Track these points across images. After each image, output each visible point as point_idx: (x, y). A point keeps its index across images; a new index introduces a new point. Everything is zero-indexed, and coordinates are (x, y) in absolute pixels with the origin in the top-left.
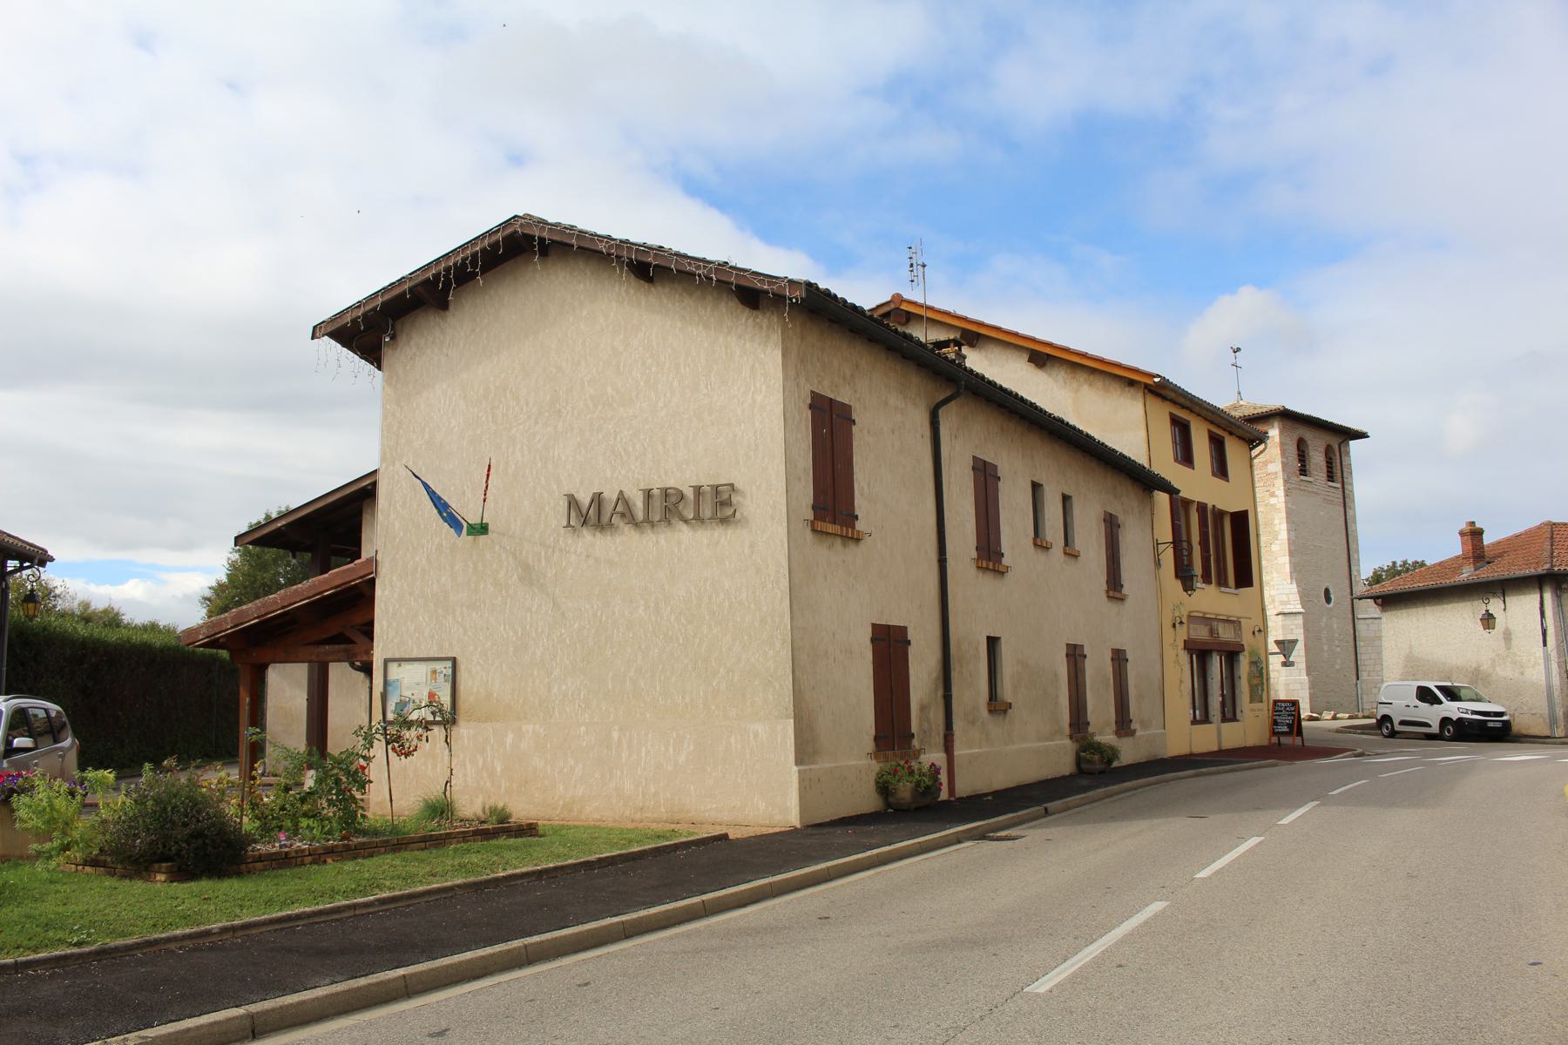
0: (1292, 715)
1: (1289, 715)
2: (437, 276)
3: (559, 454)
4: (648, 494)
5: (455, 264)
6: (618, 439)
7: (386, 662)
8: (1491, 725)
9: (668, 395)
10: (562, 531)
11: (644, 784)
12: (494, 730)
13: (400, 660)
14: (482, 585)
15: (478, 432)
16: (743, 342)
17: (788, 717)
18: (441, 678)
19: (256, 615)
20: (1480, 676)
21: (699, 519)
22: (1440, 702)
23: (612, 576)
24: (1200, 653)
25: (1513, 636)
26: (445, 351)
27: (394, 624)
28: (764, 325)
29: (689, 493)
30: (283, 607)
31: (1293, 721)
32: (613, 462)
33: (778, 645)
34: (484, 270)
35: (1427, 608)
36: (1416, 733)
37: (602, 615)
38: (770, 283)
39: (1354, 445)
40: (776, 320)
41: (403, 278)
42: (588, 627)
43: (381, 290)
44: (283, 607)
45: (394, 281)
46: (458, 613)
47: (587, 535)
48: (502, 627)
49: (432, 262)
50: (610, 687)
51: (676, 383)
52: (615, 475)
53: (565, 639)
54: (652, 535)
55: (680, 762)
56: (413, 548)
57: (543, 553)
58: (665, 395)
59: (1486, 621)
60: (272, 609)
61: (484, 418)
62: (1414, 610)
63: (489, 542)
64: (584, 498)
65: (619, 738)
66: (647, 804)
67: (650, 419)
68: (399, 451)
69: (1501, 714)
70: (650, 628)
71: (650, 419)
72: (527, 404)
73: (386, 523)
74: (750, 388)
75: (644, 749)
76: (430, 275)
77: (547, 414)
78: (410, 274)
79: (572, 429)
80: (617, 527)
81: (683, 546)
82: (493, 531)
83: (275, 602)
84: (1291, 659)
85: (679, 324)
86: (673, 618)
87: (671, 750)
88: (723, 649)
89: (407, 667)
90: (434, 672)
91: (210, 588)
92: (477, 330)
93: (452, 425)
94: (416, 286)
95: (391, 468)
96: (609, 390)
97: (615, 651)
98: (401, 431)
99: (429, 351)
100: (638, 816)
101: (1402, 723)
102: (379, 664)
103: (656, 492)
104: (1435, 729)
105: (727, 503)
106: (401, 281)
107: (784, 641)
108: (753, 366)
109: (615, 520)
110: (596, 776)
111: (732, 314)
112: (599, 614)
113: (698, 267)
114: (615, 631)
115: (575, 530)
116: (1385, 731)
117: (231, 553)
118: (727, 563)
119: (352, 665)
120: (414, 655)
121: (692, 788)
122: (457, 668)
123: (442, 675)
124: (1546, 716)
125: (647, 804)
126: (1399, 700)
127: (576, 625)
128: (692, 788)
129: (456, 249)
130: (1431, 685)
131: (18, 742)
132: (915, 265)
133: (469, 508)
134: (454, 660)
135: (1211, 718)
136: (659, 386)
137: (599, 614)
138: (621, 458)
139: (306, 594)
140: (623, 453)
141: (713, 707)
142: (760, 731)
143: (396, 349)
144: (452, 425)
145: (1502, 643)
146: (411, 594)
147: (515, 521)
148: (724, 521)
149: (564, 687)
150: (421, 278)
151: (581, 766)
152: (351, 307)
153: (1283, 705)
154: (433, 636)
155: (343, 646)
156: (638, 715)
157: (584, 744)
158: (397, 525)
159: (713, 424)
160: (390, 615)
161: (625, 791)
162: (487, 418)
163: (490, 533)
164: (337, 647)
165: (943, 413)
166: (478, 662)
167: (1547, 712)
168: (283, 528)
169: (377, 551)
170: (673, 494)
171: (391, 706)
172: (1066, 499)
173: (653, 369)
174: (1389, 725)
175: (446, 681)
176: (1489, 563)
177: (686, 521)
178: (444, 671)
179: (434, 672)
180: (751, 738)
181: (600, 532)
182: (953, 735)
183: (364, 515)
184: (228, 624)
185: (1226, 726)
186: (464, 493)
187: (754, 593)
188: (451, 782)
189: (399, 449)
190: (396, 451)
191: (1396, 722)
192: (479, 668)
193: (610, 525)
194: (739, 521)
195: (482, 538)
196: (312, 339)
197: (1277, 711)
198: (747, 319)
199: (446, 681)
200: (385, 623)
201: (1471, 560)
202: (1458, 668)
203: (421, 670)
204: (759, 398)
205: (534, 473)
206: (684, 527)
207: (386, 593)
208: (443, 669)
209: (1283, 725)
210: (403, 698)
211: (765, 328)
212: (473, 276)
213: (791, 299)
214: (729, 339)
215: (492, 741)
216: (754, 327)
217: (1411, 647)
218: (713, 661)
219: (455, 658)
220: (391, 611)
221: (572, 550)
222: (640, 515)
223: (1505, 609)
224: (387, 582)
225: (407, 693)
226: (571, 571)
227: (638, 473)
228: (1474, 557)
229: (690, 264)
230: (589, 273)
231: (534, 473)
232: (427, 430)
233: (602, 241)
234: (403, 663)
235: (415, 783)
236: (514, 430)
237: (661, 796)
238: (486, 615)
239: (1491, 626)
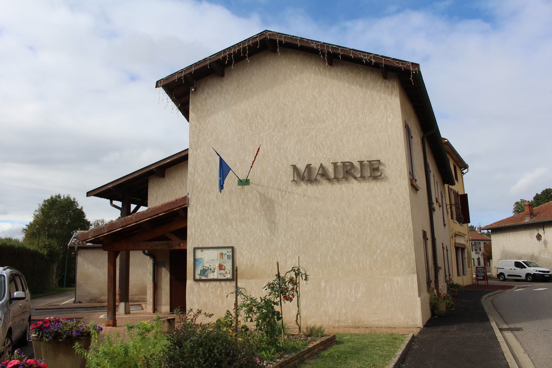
0: (484, 273)
1: (483, 273)
2: (224, 58)
3: (286, 146)
4: (335, 164)
5: (234, 52)
6: (318, 139)
7: (195, 249)
8: (546, 276)
9: (343, 118)
10: (290, 183)
11: (339, 308)
12: (256, 283)
13: (202, 249)
14: (247, 210)
15: (243, 135)
16: (380, 94)
17: (414, 273)
18: (225, 257)
19: (121, 226)
20: (534, 258)
21: (363, 177)
22: (525, 268)
23: (318, 205)
24: (457, 249)
25: (548, 243)
26: (223, 95)
27: (199, 230)
28: (390, 86)
29: (357, 165)
30: (136, 222)
31: (485, 275)
32: (315, 150)
33: (407, 238)
34: (250, 55)
35: (511, 233)
36: (517, 279)
37: (313, 225)
38: (402, 64)
40: (395, 84)
41: (206, 58)
43: (193, 64)
44: (136, 222)
45: (201, 60)
46: (234, 224)
48: (259, 231)
49: (221, 51)
50: (319, 260)
51: (346, 112)
52: (317, 156)
53: (294, 236)
54: (338, 185)
55: (358, 297)
56: (208, 192)
57: (280, 195)
58: (341, 118)
60: (130, 223)
61: (245, 128)
62: (505, 234)
63: (250, 189)
64: (302, 167)
65: (325, 286)
66: (341, 319)
67: (334, 129)
68: (199, 144)
69: (548, 272)
70: (339, 231)
71: (334, 129)
72: (269, 121)
73: (193, 179)
74: (385, 116)
75: (338, 291)
76: (221, 57)
77: (279, 126)
78: (210, 57)
79: (293, 134)
80: (319, 182)
81: (355, 191)
82: (253, 184)
83: (131, 219)
85: (347, 85)
86: (351, 226)
87: (353, 291)
88: (378, 240)
89: (206, 252)
90: (222, 254)
91: (26, 225)
92: (240, 86)
93: (228, 132)
94: (213, 62)
95: (195, 152)
96: (312, 115)
97: (321, 242)
98: (200, 135)
99: (214, 96)
100: (337, 325)
101: (509, 275)
102: (191, 250)
103: (339, 164)
104: (524, 277)
105: (377, 169)
106: (205, 60)
107: (410, 236)
108: (385, 105)
109: (319, 178)
110: (313, 305)
111: (373, 81)
113: (365, 56)
115: (297, 183)
116: (501, 279)
117: (35, 212)
118: (378, 198)
119: (144, 253)
120: (210, 245)
121: (365, 310)
122: (235, 252)
123: (226, 256)
125: (341, 319)
126: (508, 267)
127: (300, 230)
128: (365, 310)
129: (234, 45)
130: (521, 261)
131: (17, 294)
133: (239, 172)
134: (233, 248)
136: (338, 113)
138: (320, 148)
139: (149, 215)
140: (320, 145)
141: (374, 269)
142: (399, 280)
143: (196, 95)
144: (228, 132)
145: (543, 246)
146: (208, 215)
147: (264, 178)
148: (375, 178)
150: (215, 59)
151: (305, 300)
152: (177, 72)
153: (480, 269)
154: (220, 236)
155: (166, 242)
156: (335, 274)
157: (306, 289)
158: (199, 181)
159: (367, 132)
160: (196, 225)
161: (329, 312)
162: (247, 128)
163: (250, 184)
164: (162, 242)
166: (246, 249)
168: (111, 188)
169: (188, 193)
170: (348, 165)
171: (198, 272)
173: (335, 106)
174: (503, 277)
175: (228, 258)
176: (535, 216)
177: (355, 178)
178: (227, 254)
179: (222, 254)
180: (395, 284)
181: (310, 183)
182: (438, 281)
183: (149, 183)
184: (105, 230)
185: (464, 277)
186: (235, 165)
187: (393, 213)
188: (300, 314)
189: (199, 143)
190: (198, 144)
191: (506, 275)
192: (246, 252)
193: (316, 180)
194: (383, 178)
195: (246, 187)
196: (156, 87)
197: (478, 271)
198: (381, 84)
199: (228, 258)
200: (193, 230)
201: (529, 215)
202: (524, 255)
203: (216, 253)
204: (390, 120)
205: (273, 155)
206: (355, 181)
207: (194, 214)
208: (226, 253)
209: (480, 276)
210: (204, 268)
211: (390, 88)
212: (244, 58)
213: (413, 72)
214: (373, 92)
215: (255, 288)
216: (385, 87)
217: (504, 247)
218: (374, 246)
219: (233, 247)
220: (196, 223)
221: (296, 192)
222: (332, 175)
223: (544, 233)
224: (194, 209)
225: (207, 265)
226: (296, 203)
227: (329, 155)
228: (530, 214)
229: (360, 54)
230: (298, 61)
231: (273, 155)
232: (215, 134)
233: (313, 43)
234: (204, 250)
235: (212, 311)
236: (262, 134)
237: (349, 315)
238: (250, 225)
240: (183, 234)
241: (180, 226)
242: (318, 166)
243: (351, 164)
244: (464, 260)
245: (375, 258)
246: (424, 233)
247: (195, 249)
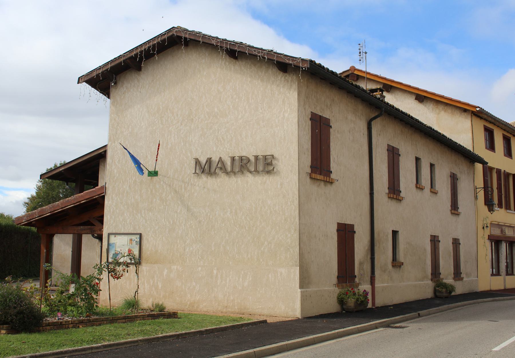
4: (233, 159)
47: (204, 177)
57: (183, 186)
64: (203, 160)
135: (501, 273)
149: (191, 249)
165: (372, 123)
172: (432, 166)
173: (237, 100)
207: (110, 202)
222: (229, 169)
245: (262, 249)
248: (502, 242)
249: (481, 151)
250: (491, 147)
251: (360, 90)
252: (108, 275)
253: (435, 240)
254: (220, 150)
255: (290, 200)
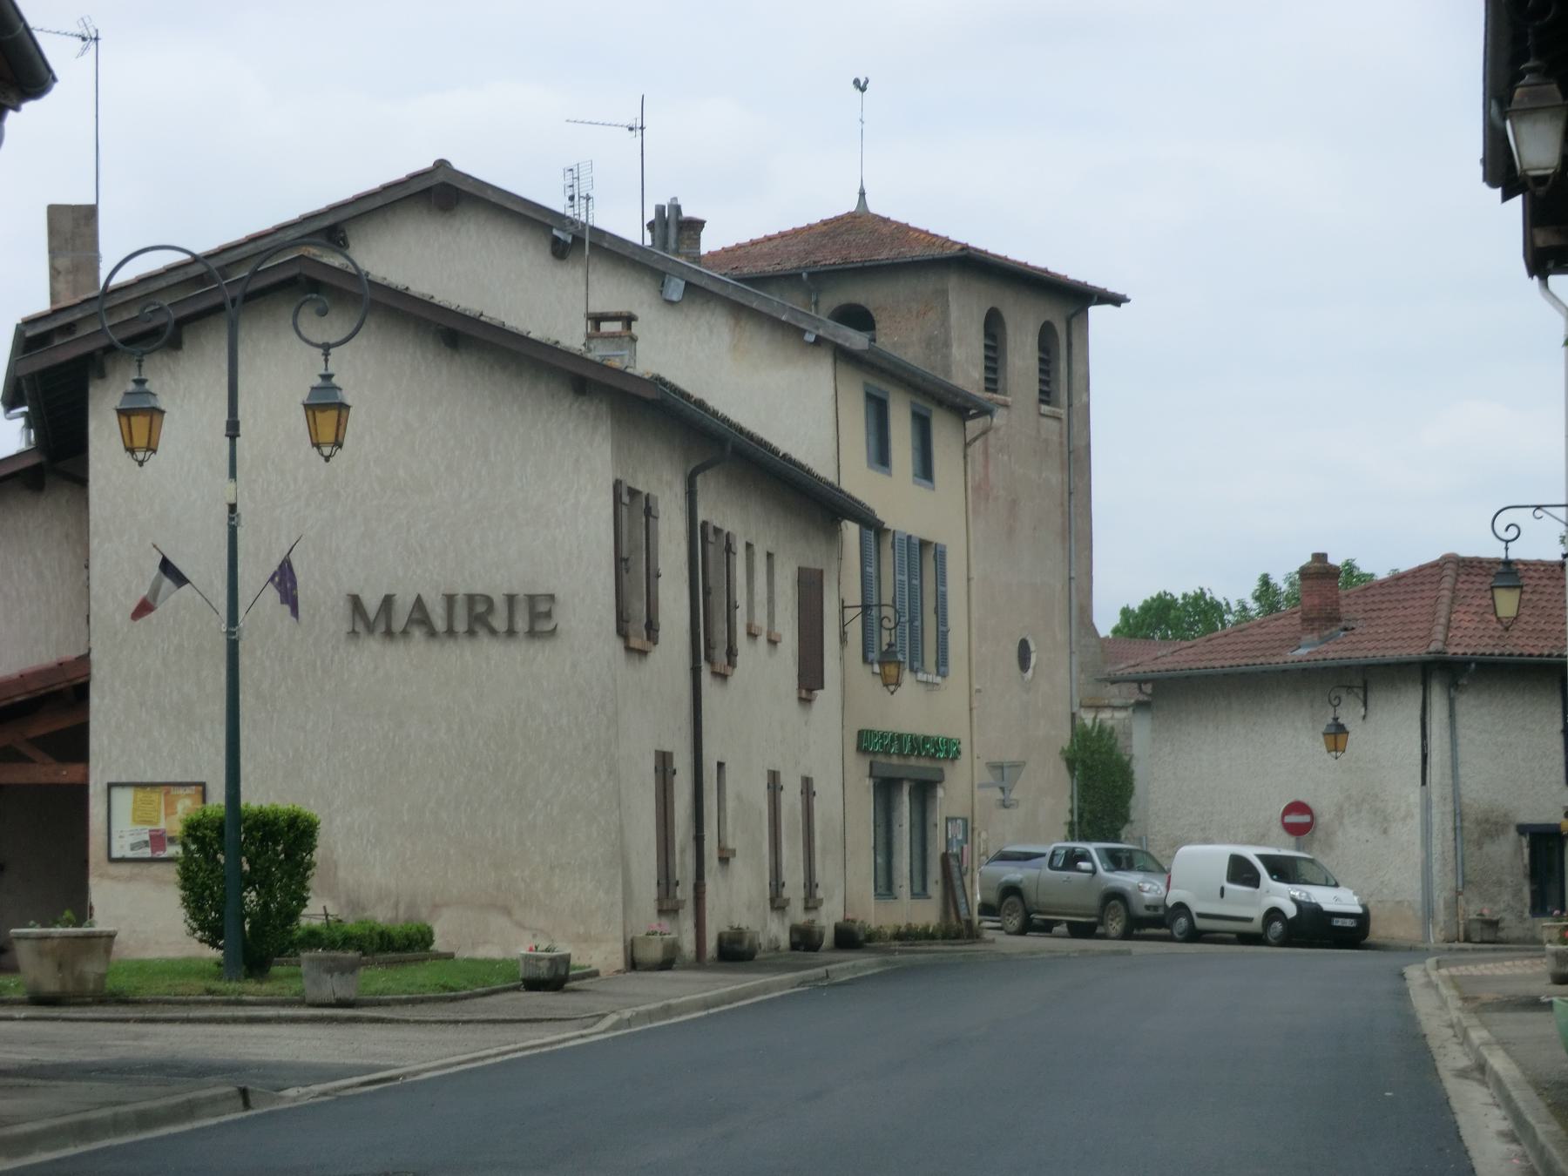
4: (450, 599)
39: (1096, 313)
42: (378, 750)
47: (373, 645)
48: (267, 748)
50: (406, 819)
57: (319, 663)
59: (1333, 737)
64: (372, 604)
81: (493, 662)
84: (1014, 796)
112: (391, 735)
114: (412, 756)
124: (1418, 906)
127: (363, 748)
130: (1250, 853)
132: (576, 198)
134: (203, 785)
135: (896, 890)
137: (391, 735)
149: (349, 819)
165: (699, 479)
167: (1419, 898)
172: (770, 556)
173: (457, 453)
177: (493, 632)
207: (107, 701)
222: (440, 624)
239: (1340, 745)
240: (75, 745)
241: (66, 722)
242: (411, 599)
243: (489, 600)
244: (930, 834)
245: (530, 817)
246: (664, 762)
247: (110, 786)
248: (902, 784)
249: (858, 481)
250: (881, 456)
251: (668, 391)
252: (945, 826)
253: (774, 777)
254: (415, 577)
255: (597, 703)
